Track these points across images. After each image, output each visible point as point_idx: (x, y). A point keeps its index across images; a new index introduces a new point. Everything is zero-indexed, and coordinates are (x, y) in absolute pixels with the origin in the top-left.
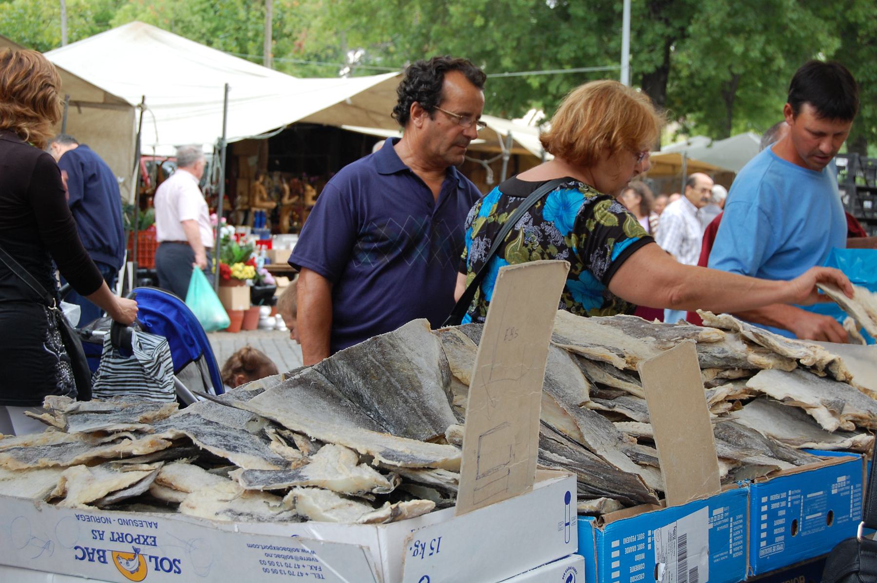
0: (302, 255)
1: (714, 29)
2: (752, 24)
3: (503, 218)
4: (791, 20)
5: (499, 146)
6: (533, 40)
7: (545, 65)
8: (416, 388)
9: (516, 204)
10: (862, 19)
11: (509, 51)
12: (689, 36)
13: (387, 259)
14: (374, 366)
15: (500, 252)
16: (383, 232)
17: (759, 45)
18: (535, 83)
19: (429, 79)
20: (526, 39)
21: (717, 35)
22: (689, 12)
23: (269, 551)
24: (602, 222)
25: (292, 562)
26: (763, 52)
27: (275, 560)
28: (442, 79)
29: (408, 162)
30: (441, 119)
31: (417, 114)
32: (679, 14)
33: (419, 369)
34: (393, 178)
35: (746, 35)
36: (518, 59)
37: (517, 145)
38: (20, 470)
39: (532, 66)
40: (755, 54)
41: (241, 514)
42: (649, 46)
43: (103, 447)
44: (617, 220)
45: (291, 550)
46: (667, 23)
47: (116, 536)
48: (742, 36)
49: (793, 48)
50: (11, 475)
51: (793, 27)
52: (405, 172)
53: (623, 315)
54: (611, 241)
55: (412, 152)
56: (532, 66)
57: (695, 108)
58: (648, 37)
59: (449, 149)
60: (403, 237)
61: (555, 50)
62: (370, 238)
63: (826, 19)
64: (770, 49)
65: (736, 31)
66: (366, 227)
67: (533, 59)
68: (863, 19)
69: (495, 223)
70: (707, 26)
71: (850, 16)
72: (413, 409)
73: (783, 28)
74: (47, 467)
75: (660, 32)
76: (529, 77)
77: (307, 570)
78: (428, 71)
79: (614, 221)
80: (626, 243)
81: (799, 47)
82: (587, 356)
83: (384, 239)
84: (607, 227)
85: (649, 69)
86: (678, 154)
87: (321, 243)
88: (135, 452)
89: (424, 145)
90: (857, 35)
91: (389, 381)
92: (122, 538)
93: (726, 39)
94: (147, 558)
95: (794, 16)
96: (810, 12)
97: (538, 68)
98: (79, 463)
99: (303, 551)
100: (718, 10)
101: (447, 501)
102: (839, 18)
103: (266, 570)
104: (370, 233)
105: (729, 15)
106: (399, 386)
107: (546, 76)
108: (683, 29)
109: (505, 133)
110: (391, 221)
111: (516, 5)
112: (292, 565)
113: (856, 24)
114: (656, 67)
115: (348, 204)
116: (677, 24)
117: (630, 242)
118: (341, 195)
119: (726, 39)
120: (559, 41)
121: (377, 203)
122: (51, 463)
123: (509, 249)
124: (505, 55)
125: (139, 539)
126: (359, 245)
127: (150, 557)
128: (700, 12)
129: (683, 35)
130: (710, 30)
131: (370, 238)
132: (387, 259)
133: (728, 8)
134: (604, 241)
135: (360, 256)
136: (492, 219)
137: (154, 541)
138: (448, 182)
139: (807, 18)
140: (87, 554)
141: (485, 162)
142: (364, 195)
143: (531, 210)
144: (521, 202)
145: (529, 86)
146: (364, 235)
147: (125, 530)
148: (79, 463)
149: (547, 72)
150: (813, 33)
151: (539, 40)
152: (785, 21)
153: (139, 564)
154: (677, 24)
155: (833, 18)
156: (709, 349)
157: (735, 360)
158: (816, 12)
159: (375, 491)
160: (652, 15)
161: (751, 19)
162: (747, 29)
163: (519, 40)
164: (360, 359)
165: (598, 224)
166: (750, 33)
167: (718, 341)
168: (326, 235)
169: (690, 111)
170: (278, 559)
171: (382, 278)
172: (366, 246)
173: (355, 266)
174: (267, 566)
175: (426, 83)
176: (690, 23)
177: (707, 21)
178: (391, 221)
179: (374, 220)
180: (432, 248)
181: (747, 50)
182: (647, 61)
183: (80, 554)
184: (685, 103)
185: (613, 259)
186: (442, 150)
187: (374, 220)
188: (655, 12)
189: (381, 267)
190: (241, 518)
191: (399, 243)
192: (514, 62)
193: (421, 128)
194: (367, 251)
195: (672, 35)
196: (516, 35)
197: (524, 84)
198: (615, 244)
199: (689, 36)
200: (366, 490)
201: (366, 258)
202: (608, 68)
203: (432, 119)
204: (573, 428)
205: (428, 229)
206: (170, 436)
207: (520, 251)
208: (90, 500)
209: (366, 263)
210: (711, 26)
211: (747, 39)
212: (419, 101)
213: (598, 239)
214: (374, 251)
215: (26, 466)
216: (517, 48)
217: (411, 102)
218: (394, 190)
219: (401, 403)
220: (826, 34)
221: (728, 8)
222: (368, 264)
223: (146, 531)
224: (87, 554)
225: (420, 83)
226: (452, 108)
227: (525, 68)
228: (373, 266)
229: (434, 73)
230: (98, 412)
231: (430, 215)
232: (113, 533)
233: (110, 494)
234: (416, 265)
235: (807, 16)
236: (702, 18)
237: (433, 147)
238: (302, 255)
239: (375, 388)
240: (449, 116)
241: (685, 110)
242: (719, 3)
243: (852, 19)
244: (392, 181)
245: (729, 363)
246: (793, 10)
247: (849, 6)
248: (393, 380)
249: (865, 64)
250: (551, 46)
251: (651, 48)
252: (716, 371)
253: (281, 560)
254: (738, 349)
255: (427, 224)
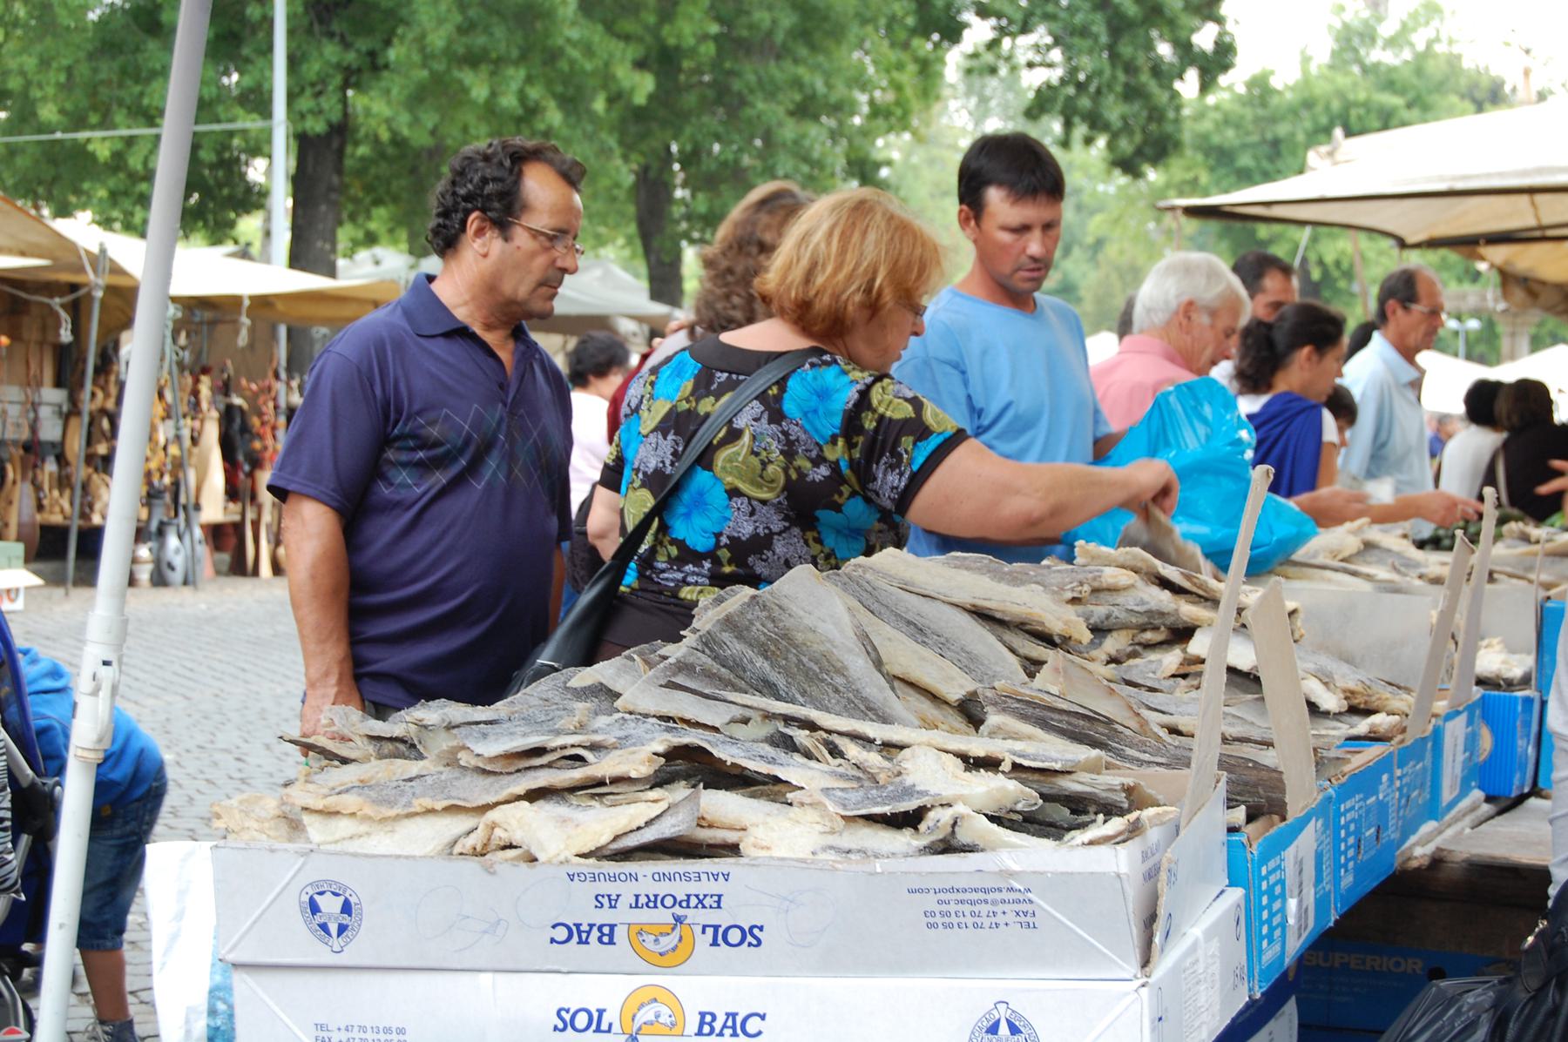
0: (294, 473)
1: (433, 56)
2: (502, 47)
3: (706, 405)
4: (569, 40)
5: (82, 270)
6: (95, 71)
7: (119, 116)
8: (841, 671)
9: (730, 386)
10: (690, 41)
11: (51, 91)
12: (386, 66)
13: (440, 478)
14: (770, 638)
15: (705, 460)
16: (434, 432)
17: (514, 86)
18: (103, 152)
19: (497, 174)
20: (83, 70)
21: (439, 66)
22: (389, 24)
23: (942, 896)
24: (888, 414)
25: (984, 909)
26: (522, 97)
27: (952, 908)
28: (520, 174)
29: (462, 314)
30: (521, 238)
31: (480, 232)
32: (363, 27)
33: (830, 641)
34: (441, 341)
35: (492, 67)
36: (68, 106)
37: (117, 270)
38: (384, 820)
39: (94, 119)
40: (509, 101)
41: (849, 852)
42: (313, 85)
43: (532, 774)
44: (910, 408)
45: (985, 891)
46: (346, 45)
47: (643, 900)
48: (485, 69)
49: (571, 91)
50: (363, 828)
51: (575, 53)
52: (461, 333)
53: (959, 554)
54: (907, 441)
55: (467, 297)
56: (94, 119)
57: (387, 198)
58: (312, 69)
59: (534, 290)
60: (468, 441)
61: (137, 89)
62: (411, 443)
63: (627, 38)
64: (534, 93)
65: (473, 60)
66: (405, 424)
67: (94, 108)
68: (691, 41)
69: (690, 413)
70: (422, 49)
71: (669, 35)
72: (850, 701)
73: (553, 56)
74: (431, 811)
75: (334, 60)
76: (89, 140)
77: (1011, 917)
78: (495, 160)
79: (907, 411)
80: (933, 443)
81: (579, 89)
82: (998, 615)
83: (437, 444)
84: (898, 421)
85: (317, 126)
86: (393, 281)
87: (328, 452)
88: (633, 775)
89: (490, 287)
90: (680, 70)
91: (800, 661)
92: (654, 902)
93: (457, 74)
94: (698, 929)
95: (574, 34)
96: (600, 28)
97: (106, 123)
98: (519, 798)
99: (1011, 889)
100: (441, 21)
101: (1084, 818)
102: (649, 39)
103: (931, 926)
104: (413, 436)
105: (463, 30)
106: (816, 668)
107: (121, 138)
108: (372, 54)
109: (95, 250)
110: (447, 416)
111: (66, 5)
112: (984, 914)
113: (677, 48)
114: (330, 125)
115: (372, 386)
116: (363, 44)
117: (939, 440)
118: (359, 371)
119: (457, 74)
120: (144, 74)
121: (420, 384)
122: (439, 806)
123: (721, 457)
124: (44, 99)
125: (688, 901)
126: (390, 455)
127: (704, 927)
128: (407, 24)
129: (374, 65)
130: (427, 57)
131: (411, 443)
132: (440, 478)
133: (458, 18)
134: (897, 442)
135: (391, 473)
136: (684, 406)
137: (719, 902)
138: (522, 347)
139: (596, 39)
140: (577, 933)
141: (56, 302)
142: (400, 372)
143: (762, 397)
144: (739, 382)
145: (92, 157)
146: (398, 438)
147: (663, 888)
148: (519, 798)
149: (125, 132)
150: (607, 65)
151: (107, 69)
152: (560, 42)
153: (681, 939)
154: (363, 44)
155: (640, 40)
156: (1120, 599)
157: (1162, 614)
158: (610, 28)
159: (1019, 807)
160: (317, 28)
161: (500, 38)
162: (494, 55)
163: (69, 70)
164: (747, 629)
165: (882, 417)
166: (498, 63)
167: (1126, 589)
168: (335, 438)
169: (378, 202)
170: (960, 907)
171: (436, 509)
172: (404, 457)
173: (385, 491)
174: (939, 919)
175: (495, 180)
176: (388, 43)
177: (421, 39)
178: (447, 416)
179: (419, 413)
180: (510, 457)
181: (494, 94)
182: (311, 111)
183: (561, 934)
184: (369, 189)
185: (915, 468)
186: (523, 291)
187: (419, 413)
188: (321, 21)
189: (433, 491)
190: (852, 856)
191: (461, 451)
192: (62, 111)
193: (485, 256)
194: (405, 465)
195: (355, 66)
196: (65, 62)
197: (80, 154)
198: (915, 444)
199: (386, 66)
200: (1009, 806)
201: (403, 476)
202: (238, 125)
203: (506, 240)
204: (1128, 714)
205: (504, 427)
206: (661, 749)
207: (743, 462)
208: (586, 850)
209: (404, 485)
210: (428, 50)
211: (493, 74)
212: (483, 210)
213: (884, 441)
214: (420, 464)
215: (392, 812)
216: (67, 87)
217: (467, 213)
218: (445, 363)
219: (832, 695)
220: (628, 65)
221: (458, 18)
222: (406, 485)
223: (706, 887)
224: (577, 933)
225: (485, 181)
226: (540, 219)
227: (79, 122)
228: (419, 491)
229: (507, 163)
230: (470, 723)
231: (505, 404)
232: (637, 896)
233: (616, 838)
234: (490, 487)
235: (595, 33)
236: (410, 36)
237: (508, 288)
238: (294, 473)
239: (788, 673)
240: (535, 234)
241: (368, 200)
242: (443, 7)
243: (672, 41)
244: (440, 347)
245: (1151, 620)
246: (573, 23)
247: (667, 14)
248: (805, 660)
249: (694, 120)
250: (129, 82)
251: (318, 88)
252: (1131, 632)
253: (967, 908)
254: (1162, 599)
255: (501, 419)
